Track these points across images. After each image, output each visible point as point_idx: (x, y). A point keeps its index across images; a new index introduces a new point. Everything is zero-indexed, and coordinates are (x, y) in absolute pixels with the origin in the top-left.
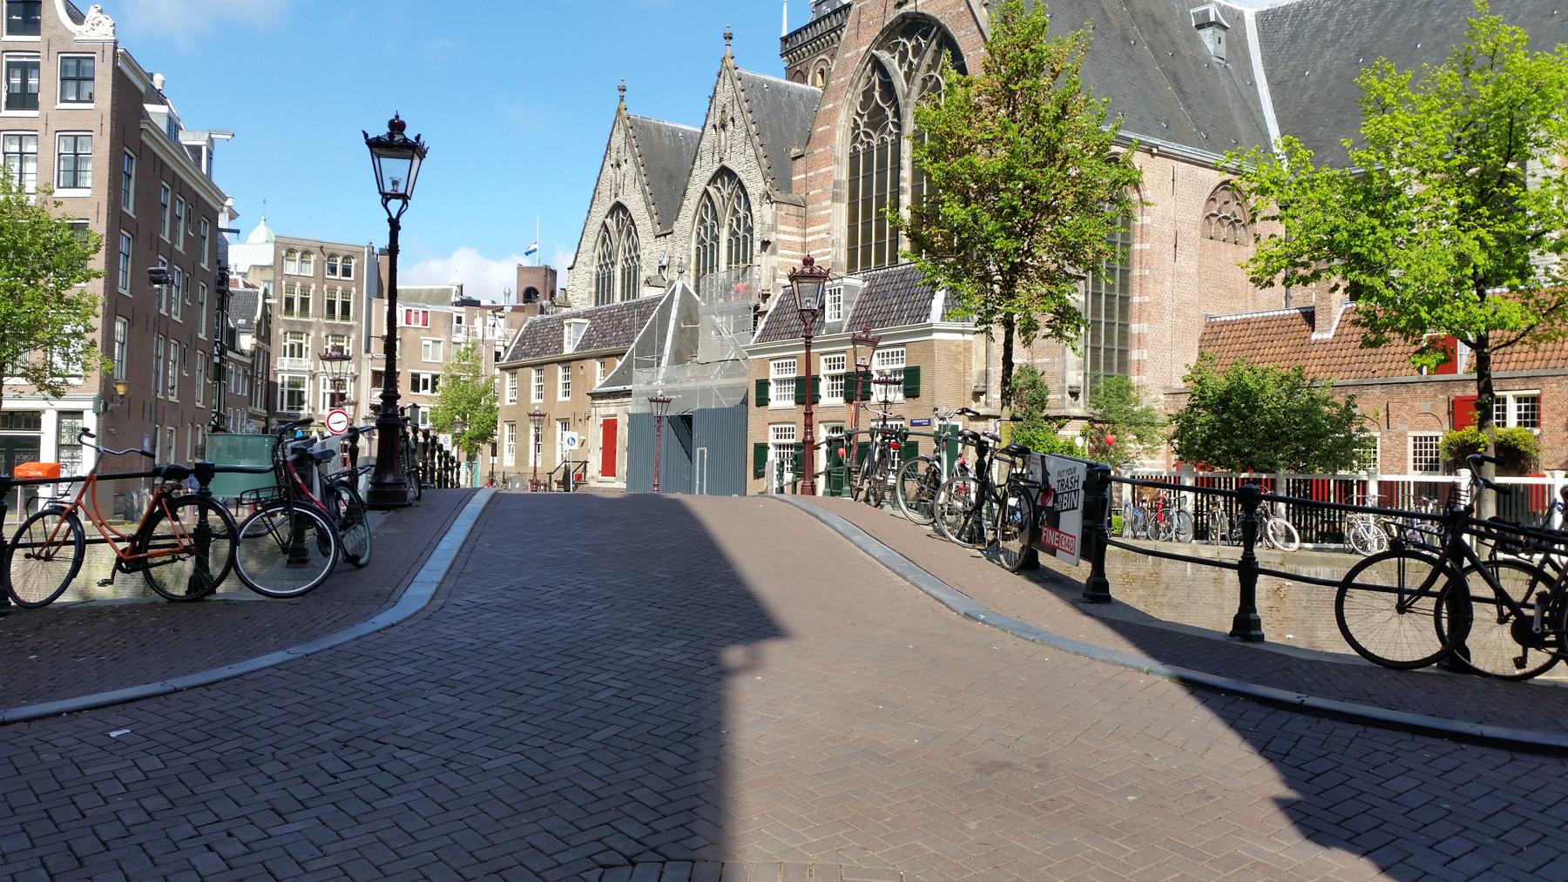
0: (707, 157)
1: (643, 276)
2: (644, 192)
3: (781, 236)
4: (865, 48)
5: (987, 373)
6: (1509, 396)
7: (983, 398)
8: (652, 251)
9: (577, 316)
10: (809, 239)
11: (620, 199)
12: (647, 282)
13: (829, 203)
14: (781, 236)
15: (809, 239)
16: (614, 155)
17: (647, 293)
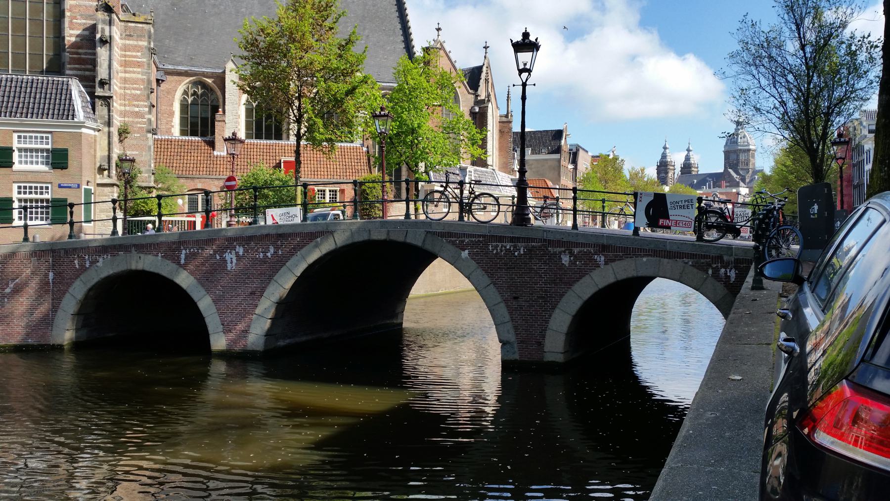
5: (109, 158)
6: (327, 189)
7: (106, 173)
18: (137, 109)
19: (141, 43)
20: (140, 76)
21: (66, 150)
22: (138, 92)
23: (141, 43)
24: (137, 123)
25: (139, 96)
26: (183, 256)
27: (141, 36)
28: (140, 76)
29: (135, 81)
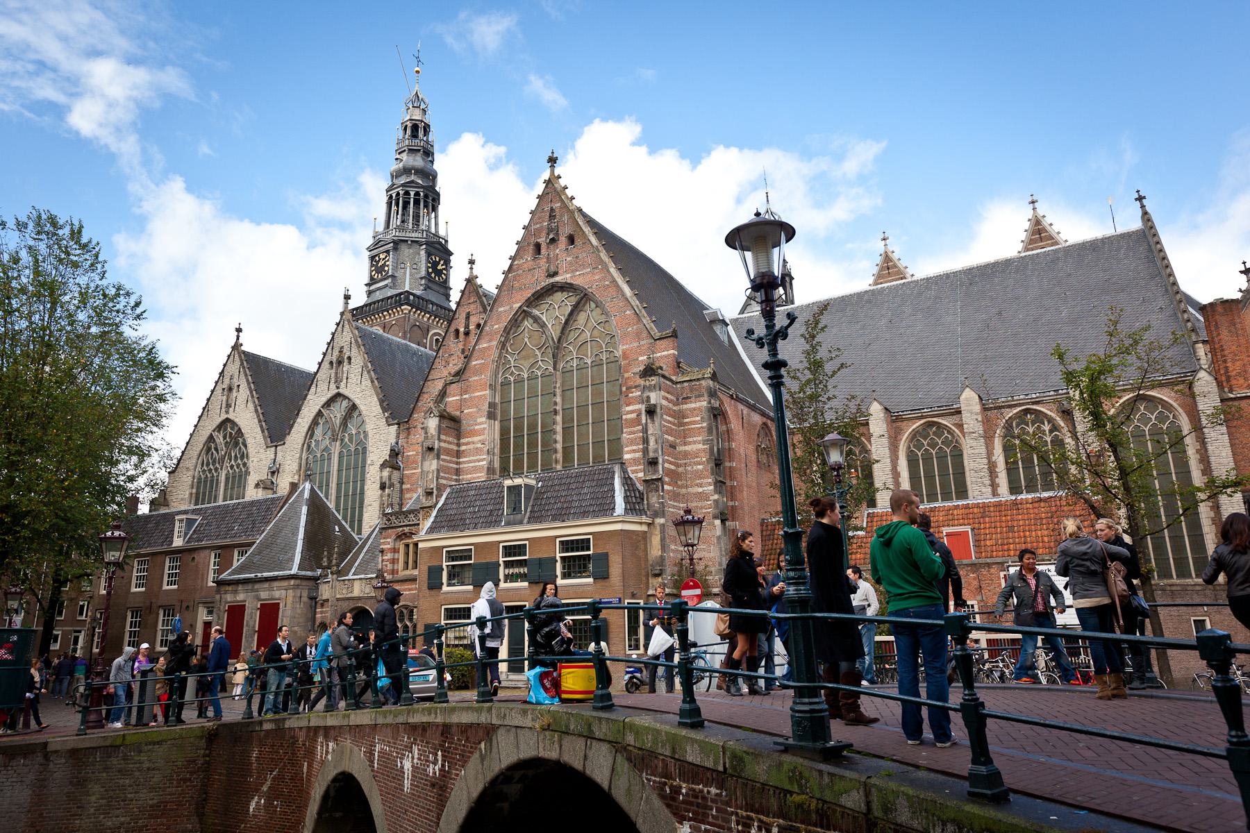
0: (322, 386)
1: (252, 480)
2: (256, 411)
3: (442, 444)
8: (259, 457)
9: (185, 512)
10: (463, 448)
11: (231, 416)
12: (257, 486)
13: (484, 419)
14: (442, 444)
15: (463, 448)
16: (227, 381)
17: (252, 494)
18: (700, 490)
19: (698, 405)
20: (700, 446)
21: (606, 555)
22: (700, 467)
23: (698, 405)
24: (702, 508)
25: (701, 471)
27: (699, 396)
28: (700, 446)
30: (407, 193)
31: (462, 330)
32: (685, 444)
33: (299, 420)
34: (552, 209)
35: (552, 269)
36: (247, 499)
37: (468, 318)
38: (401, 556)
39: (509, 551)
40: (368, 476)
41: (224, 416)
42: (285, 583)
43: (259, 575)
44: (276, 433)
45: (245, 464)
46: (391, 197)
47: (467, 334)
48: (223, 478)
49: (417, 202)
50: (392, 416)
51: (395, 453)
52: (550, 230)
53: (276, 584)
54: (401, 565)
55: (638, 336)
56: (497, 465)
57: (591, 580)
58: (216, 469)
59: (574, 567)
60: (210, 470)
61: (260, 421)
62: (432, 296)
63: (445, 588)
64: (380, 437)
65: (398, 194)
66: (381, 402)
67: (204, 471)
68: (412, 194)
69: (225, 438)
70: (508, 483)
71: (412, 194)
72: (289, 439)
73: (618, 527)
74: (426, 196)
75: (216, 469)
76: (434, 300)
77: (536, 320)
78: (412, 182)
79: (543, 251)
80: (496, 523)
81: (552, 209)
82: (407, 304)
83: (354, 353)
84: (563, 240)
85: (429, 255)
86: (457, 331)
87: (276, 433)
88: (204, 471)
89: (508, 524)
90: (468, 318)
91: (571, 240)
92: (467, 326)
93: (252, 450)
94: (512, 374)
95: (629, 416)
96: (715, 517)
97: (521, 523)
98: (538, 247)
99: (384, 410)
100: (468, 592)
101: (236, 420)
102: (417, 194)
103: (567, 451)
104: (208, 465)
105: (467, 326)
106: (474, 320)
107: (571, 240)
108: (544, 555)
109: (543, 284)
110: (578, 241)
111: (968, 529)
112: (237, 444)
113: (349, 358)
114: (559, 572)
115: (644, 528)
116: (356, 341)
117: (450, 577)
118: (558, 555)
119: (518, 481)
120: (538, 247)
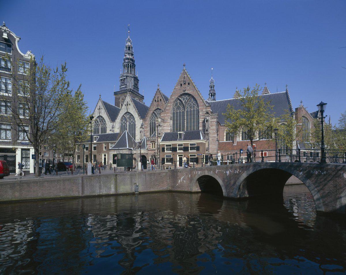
4: (176, 97)
8: (109, 124)
11: (101, 115)
19: (215, 120)
20: (215, 128)
23: (215, 120)
26: (217, 172)
28: (215, 128)
29: (214, 129)
30: (128, 64)
31: (157, 100)
32: (212, 127)
33: (118, 117)
34: (184, 77)
35: (184, 90)
36: (107, 133)
37: (158, 98)
38: (151, 146)
39: (179, 145)
40: (136, 130)
41: (99, 115)
42: (126, 150)
43: (120, 148)
44: (113, 119)
45: (105, 126)
46: (124, 65)
47: (158, 101)
48: (100, 128)
49: (131, 67)
50: (141, 118)
51: (142, 125)
52: (184, 81)
53: (123, 150)
54: (151, 147)
55: (203, 106)
56: (172, 129)
57: (196, 151)
58: (98, 127)
59: (192, 148)
60: (97, 127)
61: (108, 117)
62: (135, 90)
63: (189, 151)
64: (139, 122)
65: (126, 64)
66: (138, 114)
67: (95, 127)
68: (130, 65)
69: (99, 120)
70: (179, 132)
71: (130, 65)
72: (116, 121)
73: (202, 142)
74: (133, 66)
75: (98, 127)
76: (135, 91)
77: (180, 100)
78: (129, 62)
79: (182, 86)
80: (176, 140)
81: (184, 77)
82: (130, 92)
83: (131, 103)
84: (187, 84)
85: (134, 80)
86: (156, 101)
87: (113, 119)
88: (95, 127)
89: (179, 140)
90: (158, 98)
91: (189, 84)
92: (158, 99)
93: (107, 123)
94: (181, 110)
95: (201, 121)
96: (217, 141)
97: (182, 140)
98: (181, 85)
99: (139, 116)
100: (171, 152)
101: (102, 116)
102: (131, 65)
103: (187, 127)
104: (96, 125)
105: (158, 99)
106: (159, 98)
107: (189, 84)
108: (175, 146)
109: (182, 93)
110: (190, 84)
111: (236, 145)
112: (103, 121)
113: (130, 104)
114: (189, 149)
115: (205, 142)
116: (131, 101)
117: (166, 150)
118: (177, 147)
119: (181, 132)
120: (181, 85)
